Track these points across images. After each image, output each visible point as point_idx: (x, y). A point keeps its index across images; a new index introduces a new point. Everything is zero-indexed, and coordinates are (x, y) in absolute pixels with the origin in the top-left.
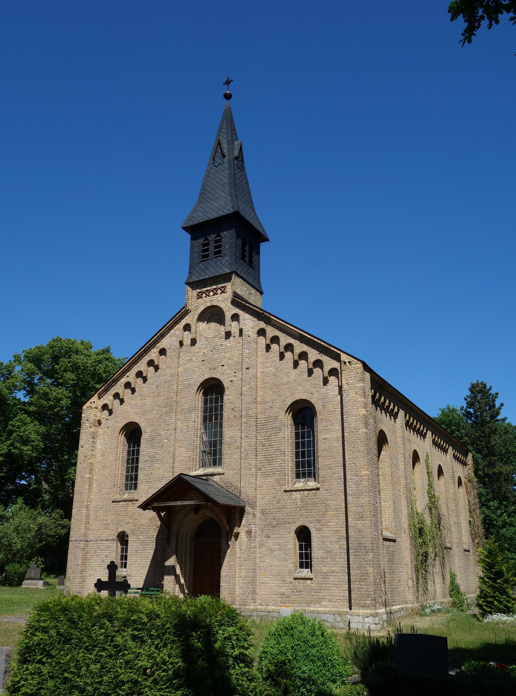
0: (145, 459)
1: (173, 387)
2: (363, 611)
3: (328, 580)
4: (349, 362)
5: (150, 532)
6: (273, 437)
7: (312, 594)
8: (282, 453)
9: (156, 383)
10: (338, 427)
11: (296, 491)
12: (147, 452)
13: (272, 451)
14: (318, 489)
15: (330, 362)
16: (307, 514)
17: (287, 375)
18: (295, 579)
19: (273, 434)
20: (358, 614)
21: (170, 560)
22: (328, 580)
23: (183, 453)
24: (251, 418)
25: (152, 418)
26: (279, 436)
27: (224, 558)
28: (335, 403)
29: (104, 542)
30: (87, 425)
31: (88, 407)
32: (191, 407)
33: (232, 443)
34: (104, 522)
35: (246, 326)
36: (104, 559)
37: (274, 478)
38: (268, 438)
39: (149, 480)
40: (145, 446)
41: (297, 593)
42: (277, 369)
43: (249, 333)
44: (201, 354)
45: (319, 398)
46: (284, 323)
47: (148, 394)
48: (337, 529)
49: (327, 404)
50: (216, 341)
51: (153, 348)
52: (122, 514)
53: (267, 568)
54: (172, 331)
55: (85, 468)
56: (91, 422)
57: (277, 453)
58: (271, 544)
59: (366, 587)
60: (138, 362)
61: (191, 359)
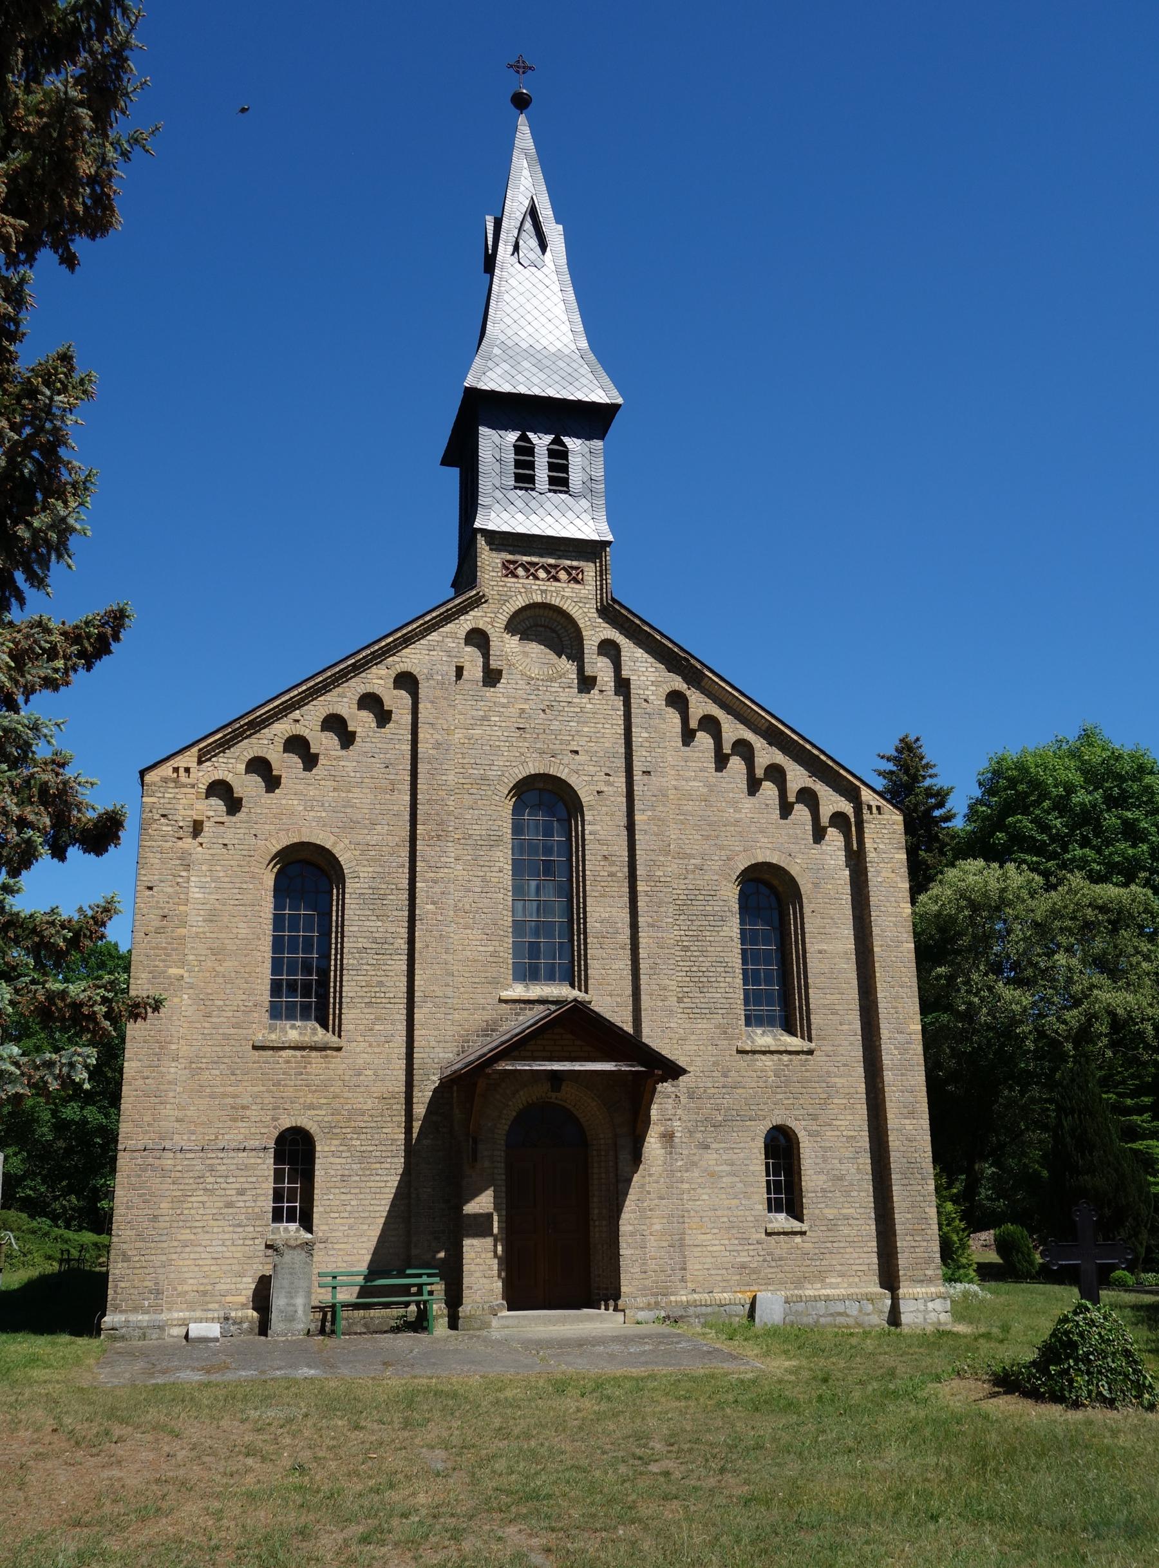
0: (360, 945)
1: (444, 778)
2: (924, 1290)
3: (837, 1234)
4: (878, 808)
5: (384, 1130)
6: (708, 934)
7: (805, 1264)
8: (730, 970)
9: (382, 756)
10: (846, 932)
11: (764, 1053)
12: (365, 929)
13: (708, 964)
14: (810, 1052)
15: (833, 798)
16: (790, 1102)
17: (734, 804)
18: (768, 1234)
19: (708, 928)
20: (916, 1296)
21: (478, 1199)
22: (837, 1234)
23: (475, 943)
24: (661, 884)
25: (374, 843)
26: (722, 934)
27: (627, 1194)
28: (839, 882)
29: (232, 1154)
30: (164, 828)
31: (165, 780)
32: (492, 833)
33: (609, 936)
34: (230, 1101)
35: (639, 676)
36: (234, 1199)
37: (713, 1021)
38: (695, 933)
39: (373, 1000)
40: (358, 912)
41: (773, 1264)
42: (711, 788)
43: (646, 692)
44: (513, 711)
45: (805, 866)
46: (736, 694)
47: (360, 780)
48: (852, 1133)
49: (822, 881)
50: (553, 689)
51: (376, 664)
52: (292, 1083)
53: (705, 1214)
54: (434, 636)
55: (165, 948)
56: (181, 824)
57: (718, 969)
58: (712, 1163)
59: (925, 1244)
60: (330, 691)
61: (485, 716)
